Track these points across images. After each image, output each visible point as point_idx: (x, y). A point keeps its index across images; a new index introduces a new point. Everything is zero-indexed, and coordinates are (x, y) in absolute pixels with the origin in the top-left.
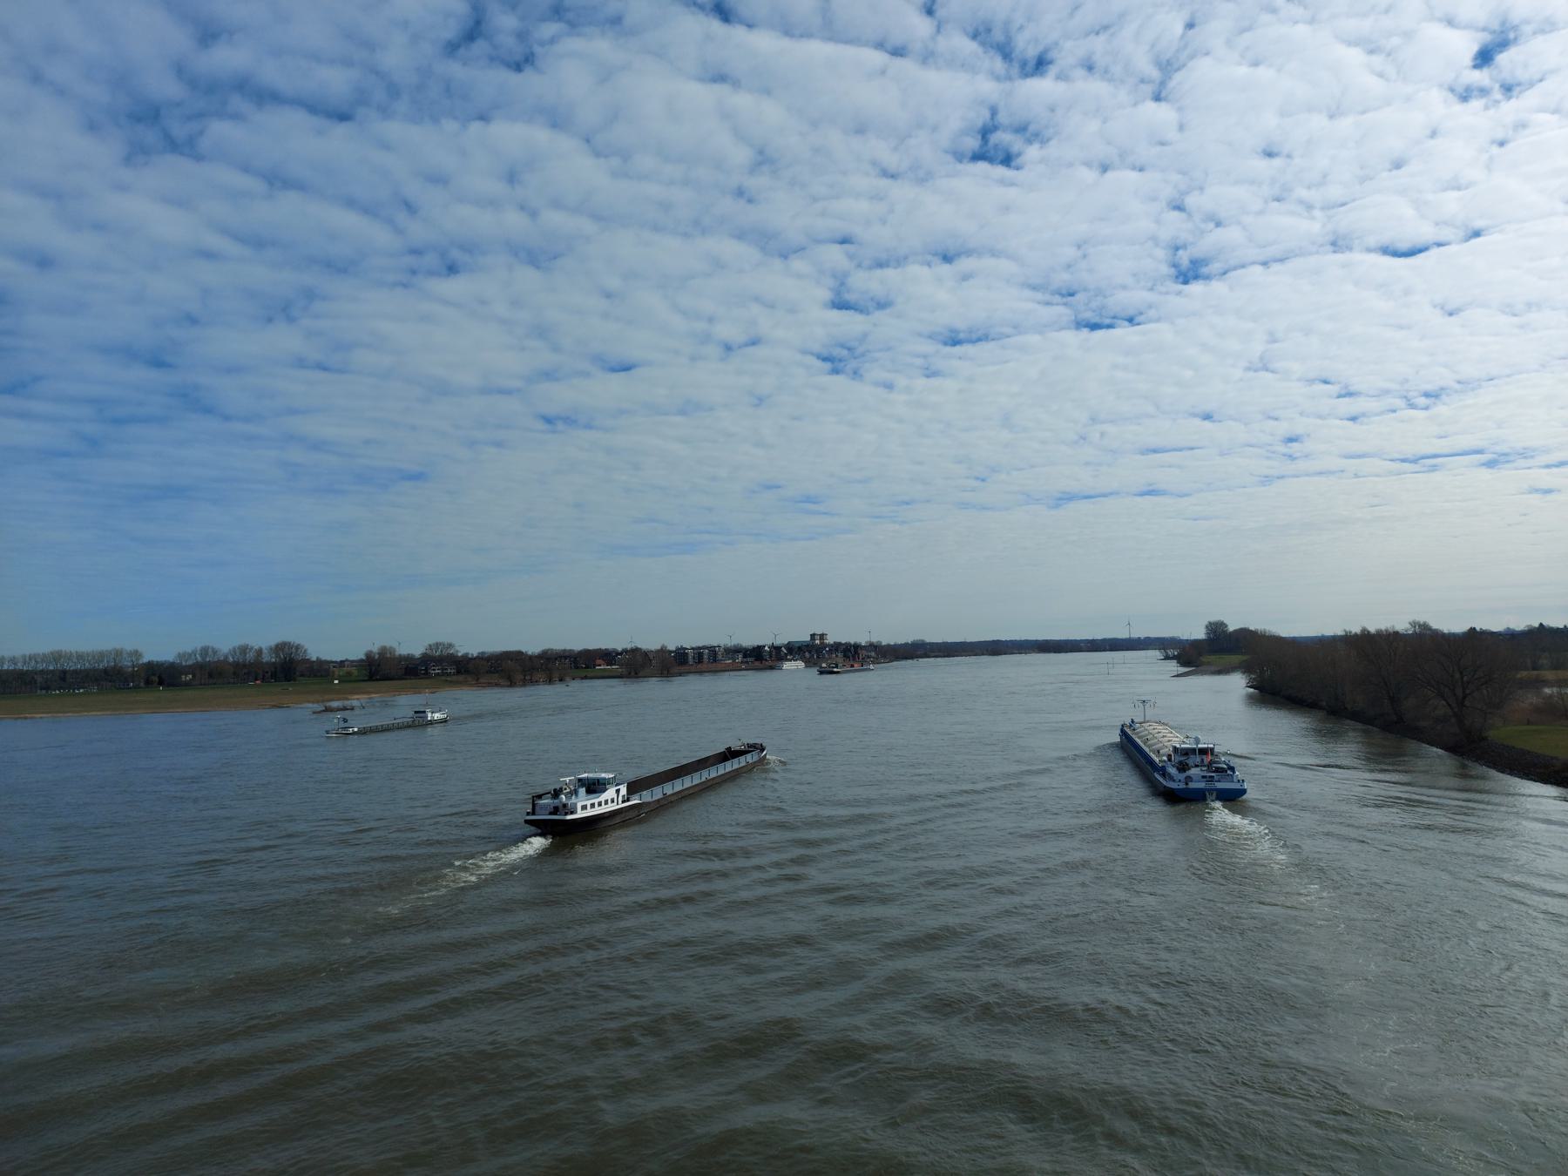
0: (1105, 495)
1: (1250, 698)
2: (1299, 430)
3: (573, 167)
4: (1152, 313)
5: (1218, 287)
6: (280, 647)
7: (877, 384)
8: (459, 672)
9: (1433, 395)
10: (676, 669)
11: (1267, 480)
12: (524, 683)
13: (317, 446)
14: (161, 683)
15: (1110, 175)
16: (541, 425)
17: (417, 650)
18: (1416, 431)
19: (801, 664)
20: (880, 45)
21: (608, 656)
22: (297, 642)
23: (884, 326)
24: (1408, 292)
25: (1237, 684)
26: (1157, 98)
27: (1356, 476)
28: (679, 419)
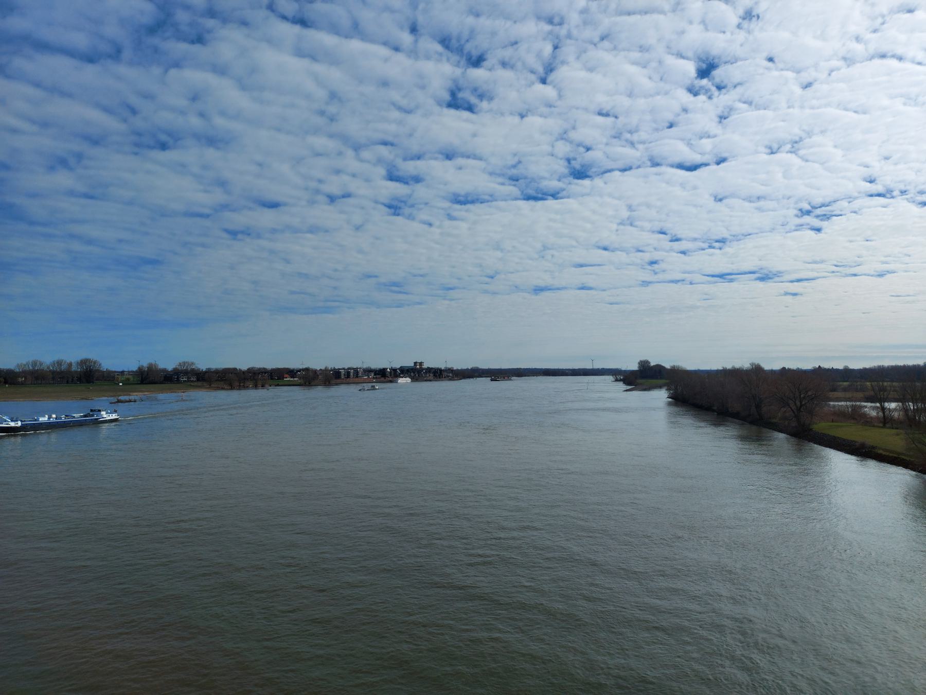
0: (558, 289)
1: (669, 404)
2: (656, 258)
3: (227, 92)
4: (564, 193)
5: (598, 182)
6: (84, 362)
7: (424, 223)
8: (198, 380)
9: (723, 241)
10: (334, 381)
11: (646, 283)
12: (240, 388)
13: (90, 242)
14: (6, 383)
15: (525, 119)
16: (225, 235)
17: (170, 367)
18: (718, 261)
19: (409, 380)
20: (385, 44)
21: (292, 373)
22: (95, 359)
23: (420, 192)
24: (695, 188)
25: (661, 396)
26: (544, 81)
27: (691, 283)
28: (309, 236)
